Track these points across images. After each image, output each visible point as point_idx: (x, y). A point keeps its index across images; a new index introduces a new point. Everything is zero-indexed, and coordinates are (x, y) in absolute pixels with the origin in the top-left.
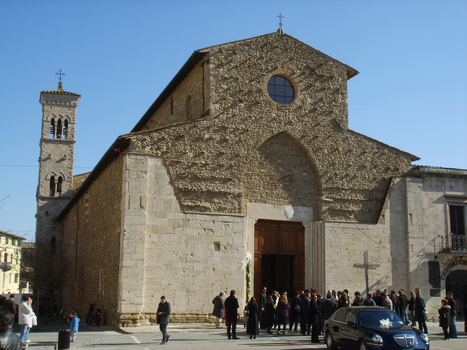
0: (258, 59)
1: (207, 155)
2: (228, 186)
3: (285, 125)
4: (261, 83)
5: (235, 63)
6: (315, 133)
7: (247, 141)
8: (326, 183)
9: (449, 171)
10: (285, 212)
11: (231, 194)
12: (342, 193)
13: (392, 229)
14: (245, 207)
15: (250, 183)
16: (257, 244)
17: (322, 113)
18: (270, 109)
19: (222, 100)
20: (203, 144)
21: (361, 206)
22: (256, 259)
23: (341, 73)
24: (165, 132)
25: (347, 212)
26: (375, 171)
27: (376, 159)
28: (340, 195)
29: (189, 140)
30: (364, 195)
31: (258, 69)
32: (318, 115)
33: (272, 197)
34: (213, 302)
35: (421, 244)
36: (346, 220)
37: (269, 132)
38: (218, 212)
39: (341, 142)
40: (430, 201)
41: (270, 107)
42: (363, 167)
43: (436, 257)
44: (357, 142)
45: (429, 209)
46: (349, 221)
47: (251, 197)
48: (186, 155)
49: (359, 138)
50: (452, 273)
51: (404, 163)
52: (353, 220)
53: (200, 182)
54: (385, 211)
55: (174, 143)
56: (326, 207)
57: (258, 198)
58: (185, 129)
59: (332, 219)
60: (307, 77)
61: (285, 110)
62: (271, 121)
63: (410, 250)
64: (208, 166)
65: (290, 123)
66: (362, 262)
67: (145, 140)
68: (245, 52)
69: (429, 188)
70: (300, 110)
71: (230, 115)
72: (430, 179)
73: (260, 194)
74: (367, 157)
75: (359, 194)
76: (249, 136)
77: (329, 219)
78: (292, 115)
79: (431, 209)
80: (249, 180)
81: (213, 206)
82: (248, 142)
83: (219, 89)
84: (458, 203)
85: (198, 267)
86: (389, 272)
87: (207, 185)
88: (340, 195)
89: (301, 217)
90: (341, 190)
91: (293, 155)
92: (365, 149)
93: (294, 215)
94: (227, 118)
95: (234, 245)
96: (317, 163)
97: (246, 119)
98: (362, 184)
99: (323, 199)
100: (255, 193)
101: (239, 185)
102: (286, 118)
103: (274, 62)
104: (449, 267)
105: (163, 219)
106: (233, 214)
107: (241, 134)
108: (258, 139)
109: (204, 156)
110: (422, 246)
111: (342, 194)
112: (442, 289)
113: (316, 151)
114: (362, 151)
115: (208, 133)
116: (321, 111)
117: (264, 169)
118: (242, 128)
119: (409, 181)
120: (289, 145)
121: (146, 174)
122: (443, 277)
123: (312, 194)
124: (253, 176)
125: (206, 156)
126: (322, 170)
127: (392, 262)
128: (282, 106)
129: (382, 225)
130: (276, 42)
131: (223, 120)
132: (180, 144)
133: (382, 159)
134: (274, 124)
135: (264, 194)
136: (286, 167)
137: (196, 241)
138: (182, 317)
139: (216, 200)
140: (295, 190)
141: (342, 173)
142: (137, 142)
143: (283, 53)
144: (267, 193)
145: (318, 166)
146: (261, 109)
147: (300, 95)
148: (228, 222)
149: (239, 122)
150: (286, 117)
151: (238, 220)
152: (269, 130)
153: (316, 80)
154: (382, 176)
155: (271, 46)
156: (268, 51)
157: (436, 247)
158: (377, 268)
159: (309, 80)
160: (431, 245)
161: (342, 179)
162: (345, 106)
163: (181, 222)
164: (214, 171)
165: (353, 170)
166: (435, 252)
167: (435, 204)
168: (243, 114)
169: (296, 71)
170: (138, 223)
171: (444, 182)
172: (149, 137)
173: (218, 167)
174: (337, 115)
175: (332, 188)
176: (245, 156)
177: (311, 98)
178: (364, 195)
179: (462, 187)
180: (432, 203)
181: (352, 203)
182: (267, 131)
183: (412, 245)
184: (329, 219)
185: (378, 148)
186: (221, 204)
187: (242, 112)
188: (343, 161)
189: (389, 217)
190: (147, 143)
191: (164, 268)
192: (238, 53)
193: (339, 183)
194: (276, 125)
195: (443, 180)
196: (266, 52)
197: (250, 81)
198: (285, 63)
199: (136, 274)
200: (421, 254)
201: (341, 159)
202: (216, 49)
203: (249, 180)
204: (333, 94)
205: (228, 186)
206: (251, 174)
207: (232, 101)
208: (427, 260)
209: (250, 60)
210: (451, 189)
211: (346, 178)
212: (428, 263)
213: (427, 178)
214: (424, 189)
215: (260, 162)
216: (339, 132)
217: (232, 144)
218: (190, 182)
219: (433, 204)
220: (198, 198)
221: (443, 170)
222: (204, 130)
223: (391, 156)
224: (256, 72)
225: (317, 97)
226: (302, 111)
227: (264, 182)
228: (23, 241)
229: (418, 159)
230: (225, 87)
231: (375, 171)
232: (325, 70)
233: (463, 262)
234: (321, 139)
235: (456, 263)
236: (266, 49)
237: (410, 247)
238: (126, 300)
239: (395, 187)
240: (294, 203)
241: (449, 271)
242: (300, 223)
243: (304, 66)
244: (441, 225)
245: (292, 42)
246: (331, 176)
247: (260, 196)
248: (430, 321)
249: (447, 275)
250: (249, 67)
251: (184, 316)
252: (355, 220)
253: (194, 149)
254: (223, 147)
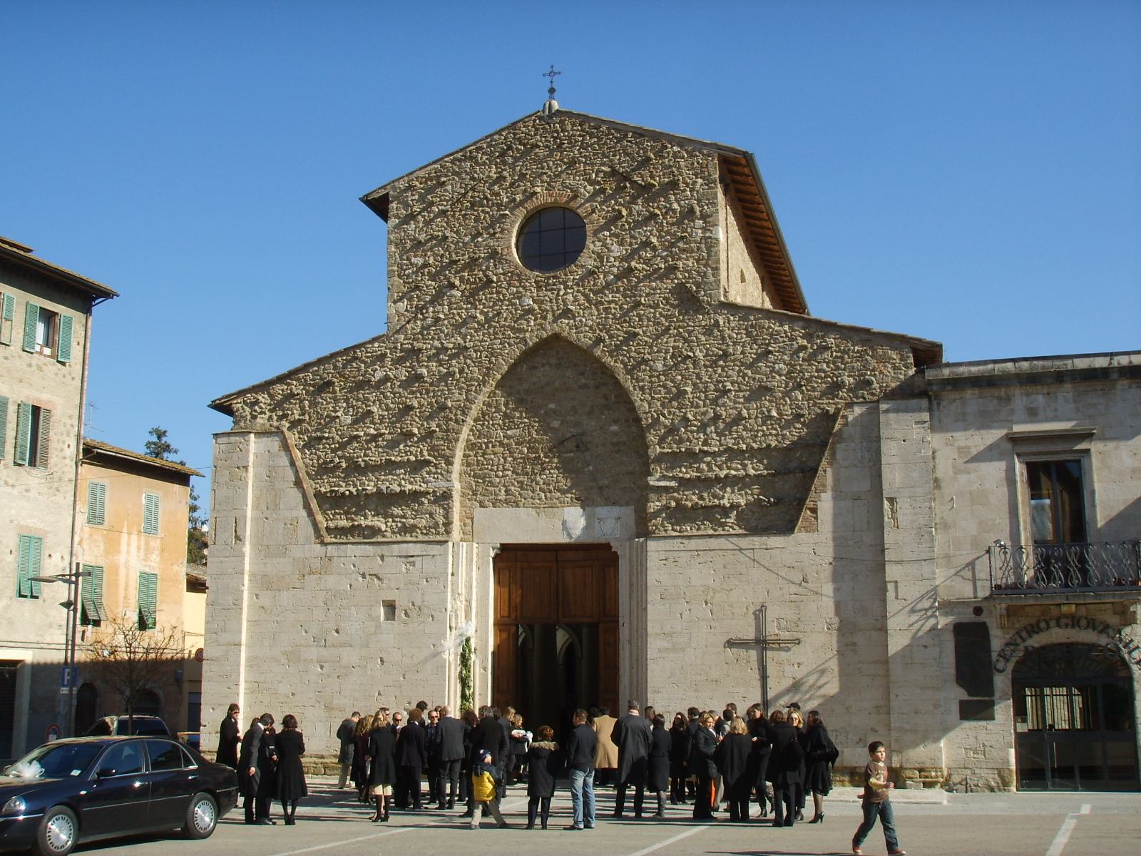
0: (495, 183)
1: (380, 415)
2: (423, 478)
3: (556, 319)
4: (497, 235)
5: (442, 205)
6: (630, 326)
7: (466, 370)
8: (659, 444)
9: (1025, 365)
10: (564, 523)
11: (428, 493)
12: (704, 462)
13: (839, 541)
14: (469, 521)
15: (482, 465)
16: (507, 603)
17: (652, 274)
18: (521, 289)
19: (413, 290)
20: (371, 393)
21: (756, 491)
22: (505, 635)
23: (702, 167)
24: (298, 380)
25: (716, 510)
26: (800, 397)
27: (801, 365)
28: (699, 470)
29: (344, 388)
30: (765, 461)
31: (493, 205)
32: (640, 281)
33: (533, 491)
34: (339, 735)
35: (926, 576)
36: (715, 530)
37: (516, 344)
38: (401, 535)
39: (700, 336)
40: (960, 457)
41: (520, 286)
42: (763, 391)
43: (978, 611)
44: (746, 329)
45: (955, 478)
46: (722, 533)
47: (484, 495)
48: (337, 420)
49: (752, 318)
50: (1029, 653)
51: (889, 362)
52: (734, 529)
53: (364, 474)
54: (820, 496)
55: (315, 399)
56: (659, 501)
57: (499, 498)
58: (335, 367)
59: (676, 531)
60: (611, 197)
61: (554, 285)
62: (522, 317)
63: (890, 594)
64: (380, 439)
65: (567, 313)
66: (750, 634)
67: (257, 402)
68: (463, 175)
69: (956, 421)
70: (594, 278)
71: (429, 321)
72: (958, 396)
73: (504, 486)
74: (774, 363)
75: (752, 460)
76: (471, 359)
77: (666, 531)
78: (573, 293)
79: (963, 478)
80: (479, 458)
81: (389, 524)
82: (467, 374)
83: (406, 269)
84: (1058, 453)
85: (350, 656)
86: (832, 655)
87: (378, 479)
88: (699, 470)
89: (605, 531)
90: (700, 456)
91: (586, 386)
92: (770, 343)
93: (586, 528)
94: (423, 328)
95: (426, 606)
96: (636, 398)
97: (464, 323)
98: (760, 434)
99: (651, 483)
100: (493, 485)
101: (448, 472)
102: (557, 303)
103: (530, 181)
104: (1021, 637)
105: (281, 560)
106: (432, 538)
107: (452, 357)
108: (490, 362)
109: (373, 418)
110: (928, 583)
111: (704, 466)
112: (1000, 698)
113: (634, 367)
114: (759, 351)
115: (383, 367)
116: (646, 271)
117: (515, 428)
118: (454, 343)
119: (887, 411)
120: (576, 365)
121: (247, 471)
123: (632, 473)
124: (487, 447)
125: (377, 417)
126: (650, 412)
127: (839, 630)
128: (548, 278)
129: (810, 534)
130: (535, 135)
131: (415, 334)
132: (326, 400)
133: (819, 363)
134: (528, 322)
135: (513, 485)
136: (568, 417)
138: (315, 763)
139: (396, 511)
140: (591, 468)
141: (704, 414)
142: (243, 409)
143: (551, 155)
144: (521, 483)
145: (638, 403)
146: (498, 293)
147: (593, 242)
148: (413, 556)
149: (448, 333)
150: (557, 300)
151: (435, 549)
152: (517, 338)
153: (634, 200)
154: (819, 408)
155: (524, 145)
156: (516, 160)
157: (979, 584)
158: (795, 648)
159: (616, 202)
160: (963, 578)
161: (703, 427)
162: (711, 246)
163: (317, 564)
164: (392, 448)
165: (735, 402)
166: (975, 597)
167: (977, 464)
168: (458, 314)
169: (582, 190)
170: (230, 571)
171: (1008, 399)
172: (266, 396)
173: (402, 437)
174: (689, 272)
175: (673, 453)
176: (460, 406)
177: (621, 243)
178: (765, 461)
179: (1072, 406)
180: (966, 462)
181: (732, 486)
182: (512, 341)
183: (896, 582)
184: (666, 531)
185: (808, 337)
186: (406, 519)
187: (455, 309)
188: (707, 382)
189: (831, 512)
190: (261, 408)
191: (283, 661)
192: (449, 180)
193: (697, 439)
194: (532, 323)
196: (513, 164)
197: (474, 237)
198: (556, 176)
200: (926, 604)
201: (701, 379)
202: (402, 185)
203: (479, 458)
204: (679, 223)
205: (423, 478)
206: (485, 443)
207: (434, 288)
208: (943, 621)
209: (473, 189)
210: (1032, 414)
211: (715, 424)
212: (952, 627)
213: (949, 395)
214: (936, 426)
215: (505, 413)
216: (697, 312)
217: (431, 384)
218: (344, 478)
219: (966, 465)
220: (360, 510)
221: (1004, 365)
222: (373, 363)
223: (849, 350)
224: (488, 213)
225: (635, 238)
226: (599, 278)
227: (515, 459)
230: (419, 261)
231: (800, 397)
232: (658, 168)
233: (1069, 621)
234: (648, 337)
235: (1043, 625)
236: (511, 156)
237: (890, 587)
239: (848, 431)
240: (587, 498)
241: (1021, 647)
243: (605, 173)
244: (997, 521)
245: (573, 125)
246: (672, 423)
247: (505, 491)
248: (959, 786)
250: (473, 205)
251: (321, 760)
252: (741, 528)
253: (353, 407)
254: (413, 393)
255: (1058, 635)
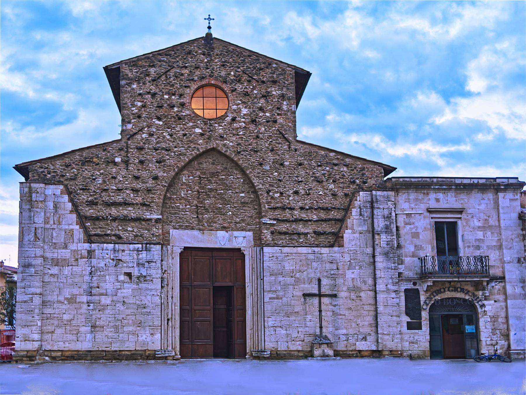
50: (437, 301)
85: (105, 300)
105: (64, 251)
122: (424, 307)
137: (102, 273)
191: (66, 302)
195: (425, 192)
199: (31, 309)
228: (429, 265)
229: (395, 169)
233: (453, 289)
235: (442, 290)
238: (20, 337)
241: (433, 299)
242: (239, 250)
249: (430, 305)
255: (448, 294)
